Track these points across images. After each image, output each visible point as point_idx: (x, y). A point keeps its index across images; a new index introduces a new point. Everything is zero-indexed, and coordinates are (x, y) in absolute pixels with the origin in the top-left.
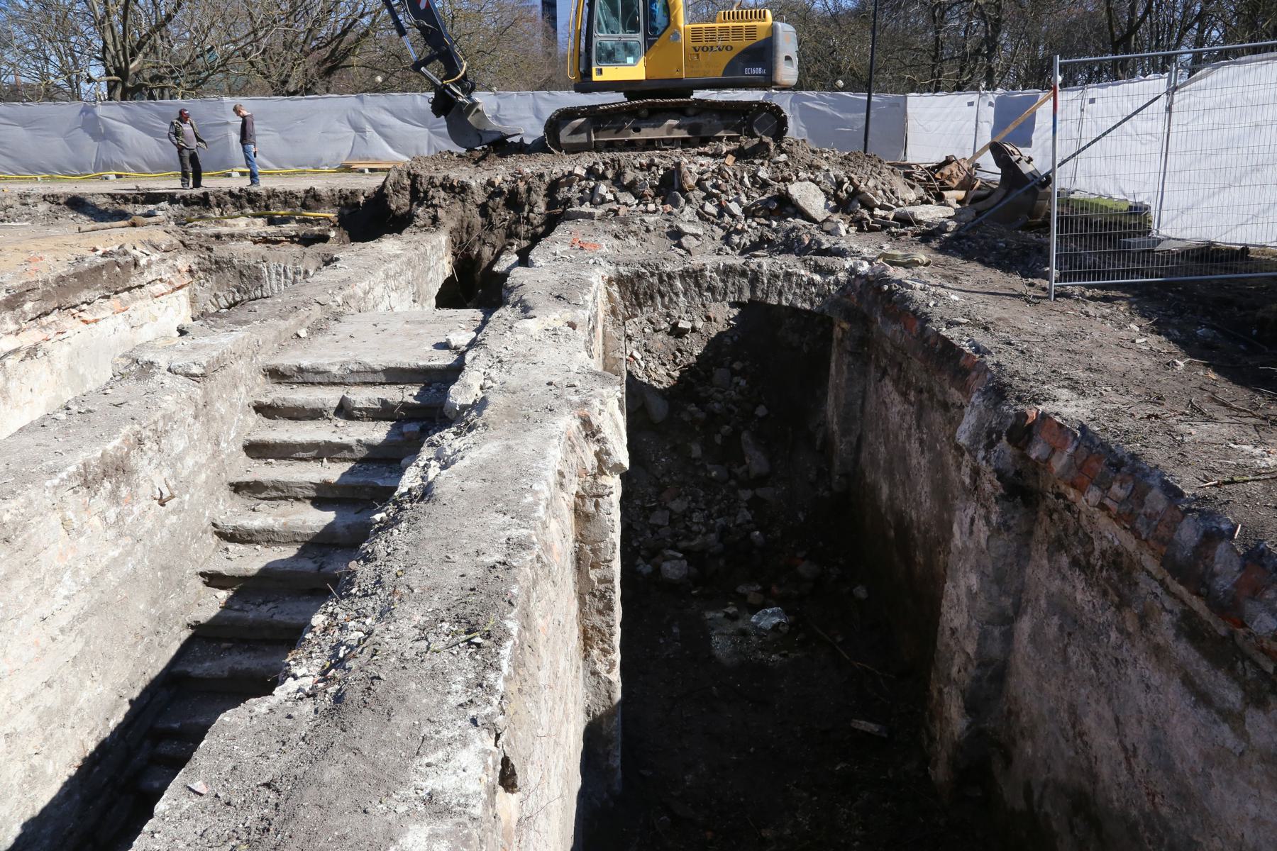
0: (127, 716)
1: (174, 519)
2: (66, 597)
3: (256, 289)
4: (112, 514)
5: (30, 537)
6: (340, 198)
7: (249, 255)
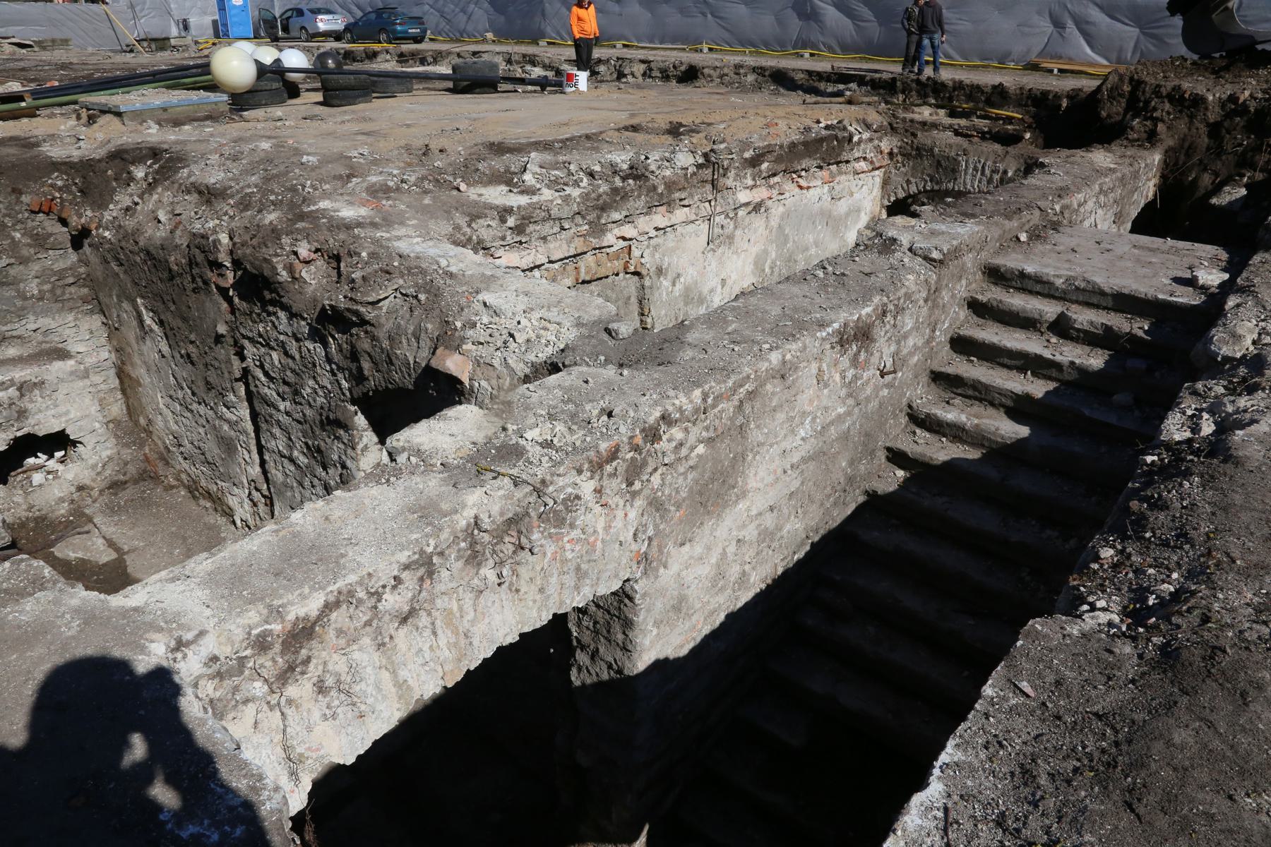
0: (807, 554)
1: (885, 392)
2: (803, 439)
3: (949, 182)
4: (850, 373)
5: (797, 378)
6: (1028, 98)
7: (951, 146)
